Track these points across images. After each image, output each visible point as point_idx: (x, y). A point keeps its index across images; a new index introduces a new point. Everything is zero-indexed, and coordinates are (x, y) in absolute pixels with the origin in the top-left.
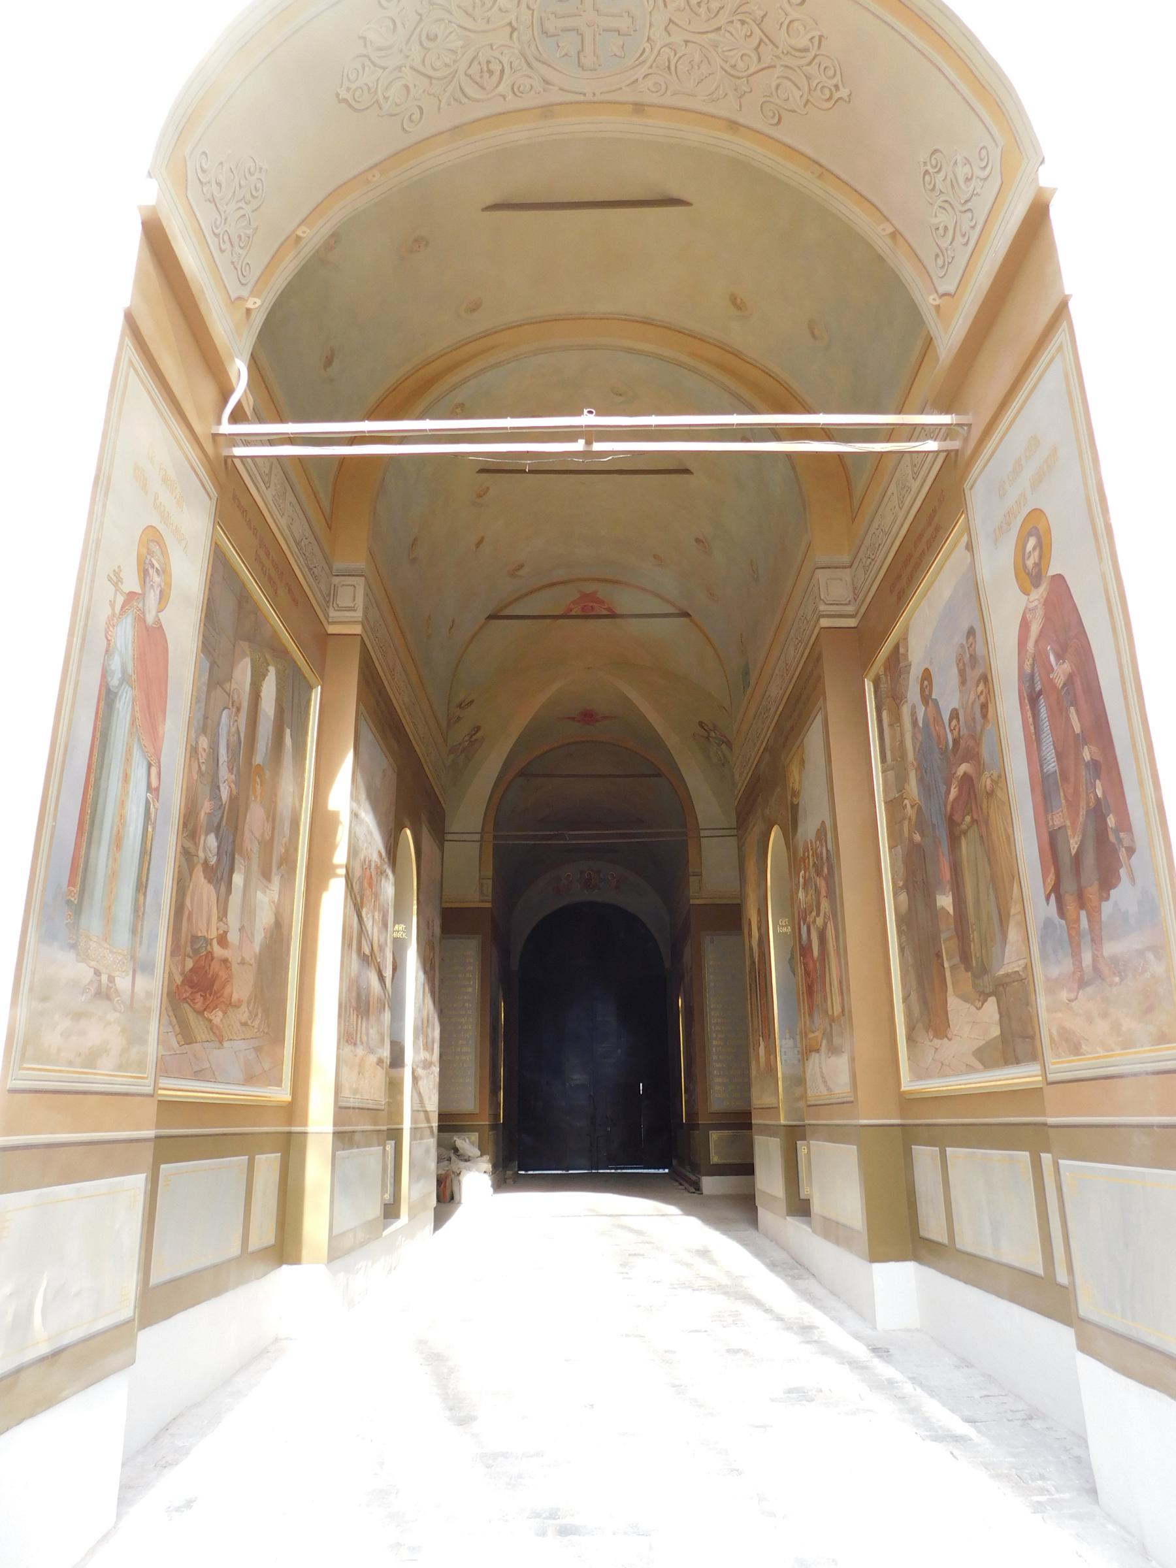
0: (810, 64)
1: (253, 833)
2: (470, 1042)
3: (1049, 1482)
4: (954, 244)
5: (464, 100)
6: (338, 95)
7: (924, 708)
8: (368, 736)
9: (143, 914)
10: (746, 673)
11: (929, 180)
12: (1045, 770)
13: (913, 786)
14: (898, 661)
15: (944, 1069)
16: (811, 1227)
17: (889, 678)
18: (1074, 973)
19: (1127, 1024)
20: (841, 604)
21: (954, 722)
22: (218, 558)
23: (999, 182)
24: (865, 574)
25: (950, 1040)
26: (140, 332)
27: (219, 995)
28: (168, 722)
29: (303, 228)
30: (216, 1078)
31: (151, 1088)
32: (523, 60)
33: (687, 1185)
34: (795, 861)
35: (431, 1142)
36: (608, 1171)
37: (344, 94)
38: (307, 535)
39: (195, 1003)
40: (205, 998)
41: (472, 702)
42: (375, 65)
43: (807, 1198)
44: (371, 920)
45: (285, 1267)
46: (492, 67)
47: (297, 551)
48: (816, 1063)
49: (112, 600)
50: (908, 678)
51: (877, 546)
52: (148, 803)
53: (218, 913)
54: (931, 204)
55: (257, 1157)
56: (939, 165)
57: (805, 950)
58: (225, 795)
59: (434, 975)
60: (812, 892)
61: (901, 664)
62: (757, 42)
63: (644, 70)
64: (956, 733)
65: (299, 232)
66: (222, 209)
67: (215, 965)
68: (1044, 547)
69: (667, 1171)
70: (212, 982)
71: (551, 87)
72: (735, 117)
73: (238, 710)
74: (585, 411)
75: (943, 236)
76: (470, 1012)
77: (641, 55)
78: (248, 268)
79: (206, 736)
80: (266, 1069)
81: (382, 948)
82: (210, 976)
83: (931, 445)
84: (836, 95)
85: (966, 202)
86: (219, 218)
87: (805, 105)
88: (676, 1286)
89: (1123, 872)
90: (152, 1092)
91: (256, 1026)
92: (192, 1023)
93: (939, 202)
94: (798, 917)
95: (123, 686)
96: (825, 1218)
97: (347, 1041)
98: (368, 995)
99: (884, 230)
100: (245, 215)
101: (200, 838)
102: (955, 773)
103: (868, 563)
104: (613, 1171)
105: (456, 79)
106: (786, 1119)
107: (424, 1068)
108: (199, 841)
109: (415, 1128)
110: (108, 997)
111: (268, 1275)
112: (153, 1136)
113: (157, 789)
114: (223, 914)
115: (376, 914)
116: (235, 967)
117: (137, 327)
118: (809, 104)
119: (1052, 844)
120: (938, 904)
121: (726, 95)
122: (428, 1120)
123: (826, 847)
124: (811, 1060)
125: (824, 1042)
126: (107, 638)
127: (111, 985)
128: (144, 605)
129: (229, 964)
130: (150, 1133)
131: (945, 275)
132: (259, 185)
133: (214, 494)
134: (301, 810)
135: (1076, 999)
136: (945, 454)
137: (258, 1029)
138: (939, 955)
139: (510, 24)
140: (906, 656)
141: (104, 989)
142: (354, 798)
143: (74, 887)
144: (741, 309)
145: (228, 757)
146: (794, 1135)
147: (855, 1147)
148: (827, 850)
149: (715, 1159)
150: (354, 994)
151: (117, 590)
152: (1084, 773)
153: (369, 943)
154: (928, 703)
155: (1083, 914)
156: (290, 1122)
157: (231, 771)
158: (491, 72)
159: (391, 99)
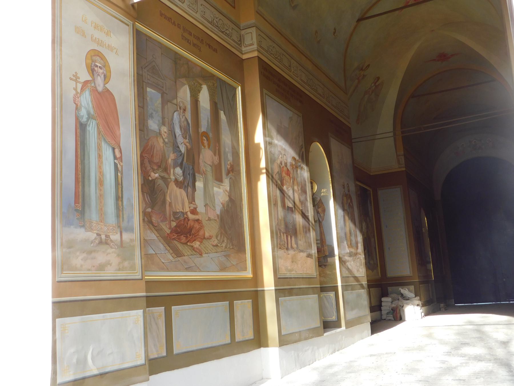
8: (273, 104)
27: (196, 235)
38: (217, 16)
40: (187, 237)
41: (369, 65)
45: (262, 348)
52: (116, 165)
58: (183, 149)
70: (191, 229)
73: (185, 110)
79: (165, 126)
90: (141, 278)
92: (180, 248)
95: (90, 120)
110: (106, 243)
116: (204, 222)
141: (104, 241)
143: (78, 204)
156: (257, 287)
157: (185, 138)
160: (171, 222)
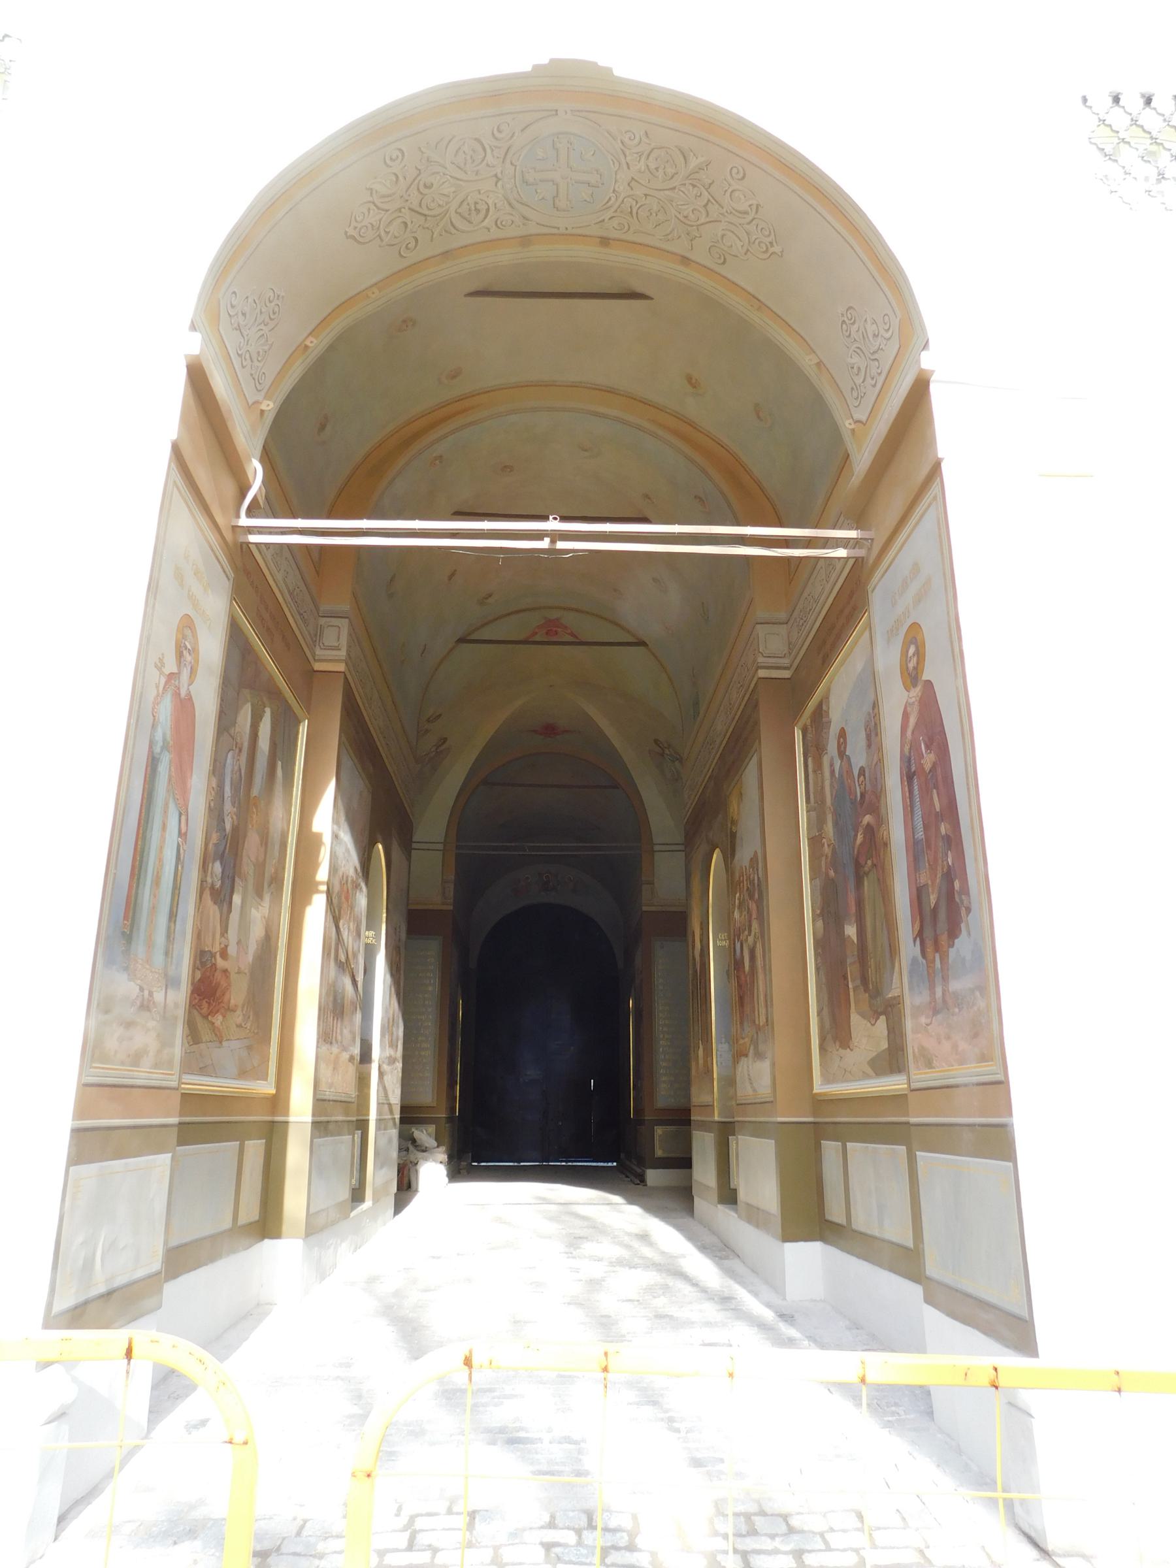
0: (749, 223)
1: (249, 858)
2: (430, 1039)
3: (901, 1408)
4: (865, 383)
5: (453, 231)
6: (346, 233)
7: (839, 761)
8: (348, 763)
9: (173, 939)
10: (696, 704)
11: (846, 328)
12: (916, 837)
13: (829, 828)
14: (821, 715)
15: (847, 1075)
16: (737, 1213)
17: (814, 729)
18: (930, 1003)
19: (963, 1046)
20: (777, 657)
21: (862, 778)
22: (235, 633)
23: (898, 346)
24: (799, 633)
25: (852, 1050)
26: (182, 456)
27: (220, 1001)
28: (194, 776)
29: (311, 338)
30: (216, 1074)
31: (177, 1082)
32: (506, 202)
33: (632, 1178)
34: (732, 883)
35: (394, 1133)
36: (559, 1164)
37: (351, 232)
39: (201, 1009)
40: (209, 1003)
42: (378, 208)
43: (735, 1188)
44: (347, 930)
45: (266, 1241)
46: (478, 207)
47: (290, 600)
48: (744, 1065)
49: (157, 682)
50: (829, 732)
51: (808, 609)
53: (221, 930)
54: (848, 347)
55: (246, 1142)
56: (853, 319)
57: (738, 964)
58: (228, 826)
59: (399, 978)
60: (745, 913)
61: (824, 719)
62: (706, 202)
63: (610, 213)
64: (862, 787)
65: (308, 343)
66: (245, 333)
67: (218, 975)
68: (920, 655)
69: (615, 1164)
71: (530, 222)
72: (687, 255)
73: (240, 750)
74: (551, 517)
75: (857, 375)
76: (430, 1010)
77: (608, 202)
78: (263, 378)
80: (256, 1065)
81: (355, 955)
82: (214, 984)
83: (842, 553)
84: (771, 250)
85: (874, 352)
86: (242, 341)
87: (746, 254)
88: (614, 1264)
89: (963, 926)
91: (248, 1028)
93: (853, 348)
94: (735, 935)
96: (748, 1204)
97: (325, 1041)
98: (343, 998)
99: (810, 360)
100: (263, 335)
101: (208, 866)
102: (861, 822)
103: (801, 624)
104: (564, 1164)
105: (447, 215)
106: (718, 1117)
107: (389, 1064)
108: (208, 869)
109: (380, 1120)
110: (148, 1009)
111: (253, 1248)
112: (177, 1122)
113: (186, 834)
114: (225, 930)
115: (351, 924)
116: (233, 976)
117: (180, 452)
118: (749, 253)
119: (919, 896)
120: (846, 933)
121: (680, 237)
122: (391, 1112)
123: (758, 875)
124: (741, 1063)
125: (752, 1047)
126: (153, 714)
127: (150, 999)
128: (179, 682)
129: (228, 974)
130: (174, 1120)
131: (859, 405)
132: (276, 309)
133: (231, 575)
134: (288, 833)
135: (931, 1023)
136: (854, 560)
137: (250, 1030)
138: (845, 977)
139: (496, 176)
140: (827, 712)
141: (145, 1003)
142: (335, 821)
144: (695, 387)
145: (231, 792)
146: (726, 1131)
147: (773, 1141)
148: (758, 878)
149: (659, 1153)
150: (331, 998)
151: (161, 674)
152: (941, 844)
153: (344, 951)
154: (843, 759)
155: (937, 956)
157: (233, 804)
158: (478, 211)
159: (391, 232)
160: (196, 970)
